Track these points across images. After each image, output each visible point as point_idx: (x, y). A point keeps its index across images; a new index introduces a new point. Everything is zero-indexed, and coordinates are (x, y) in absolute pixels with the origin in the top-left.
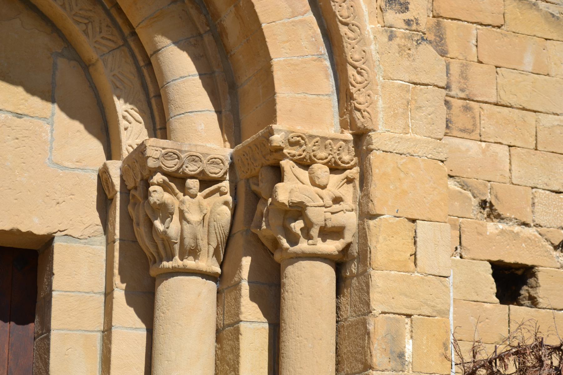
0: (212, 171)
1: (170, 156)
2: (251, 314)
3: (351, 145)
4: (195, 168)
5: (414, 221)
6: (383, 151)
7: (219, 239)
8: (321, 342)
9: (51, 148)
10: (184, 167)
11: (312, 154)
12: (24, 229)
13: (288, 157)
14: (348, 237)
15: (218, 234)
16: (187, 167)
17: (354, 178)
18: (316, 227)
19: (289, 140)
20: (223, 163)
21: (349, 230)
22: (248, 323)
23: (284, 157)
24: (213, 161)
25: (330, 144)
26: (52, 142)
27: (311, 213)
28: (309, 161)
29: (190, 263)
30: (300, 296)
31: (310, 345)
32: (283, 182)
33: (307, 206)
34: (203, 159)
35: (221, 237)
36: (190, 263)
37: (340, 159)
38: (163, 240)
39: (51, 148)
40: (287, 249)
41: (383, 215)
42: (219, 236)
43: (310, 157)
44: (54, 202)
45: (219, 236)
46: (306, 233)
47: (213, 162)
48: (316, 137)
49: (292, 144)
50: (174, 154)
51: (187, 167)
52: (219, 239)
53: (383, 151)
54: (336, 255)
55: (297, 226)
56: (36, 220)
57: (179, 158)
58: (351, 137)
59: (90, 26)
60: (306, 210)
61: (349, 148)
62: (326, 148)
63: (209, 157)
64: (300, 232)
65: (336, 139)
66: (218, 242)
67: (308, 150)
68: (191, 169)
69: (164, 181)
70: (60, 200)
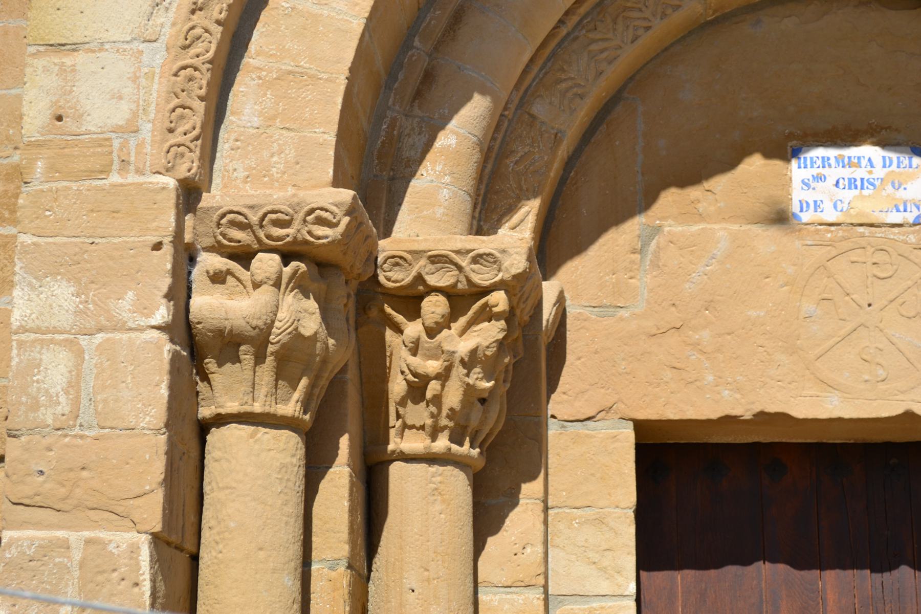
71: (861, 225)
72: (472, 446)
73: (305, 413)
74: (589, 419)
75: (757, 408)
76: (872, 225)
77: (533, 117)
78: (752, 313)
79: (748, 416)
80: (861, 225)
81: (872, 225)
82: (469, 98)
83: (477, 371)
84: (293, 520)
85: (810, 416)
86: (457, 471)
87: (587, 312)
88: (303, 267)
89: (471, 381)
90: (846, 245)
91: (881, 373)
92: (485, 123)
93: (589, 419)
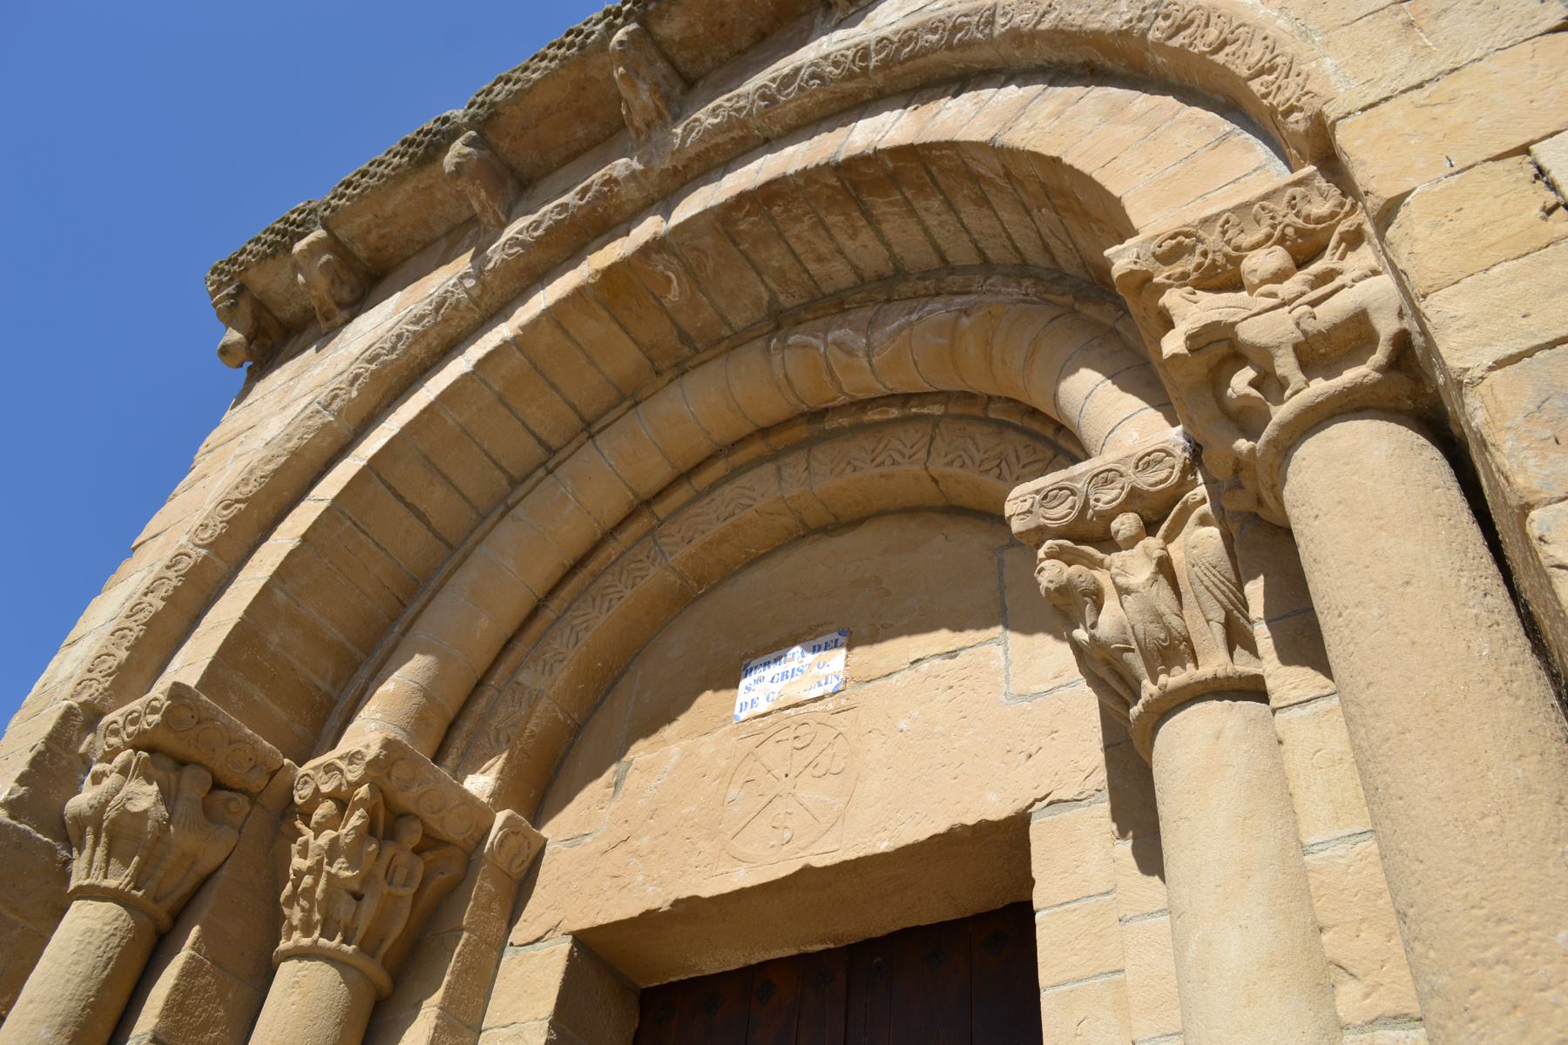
0: (1153, 480)
1: (1055, 497)
2: (830, 424)
3: (1321, 182)
4: (1114, 493)
5: (1524, 150)
6: (1363, 110)
7: (1222, 597)
8: (1409, 589)
9: (1007, 678)
10: (1092, 502)
11: (1228, 249)
12: (970, 820)
13: (1170, 286)
14: (1386, 327)
15: (1212, 588)
16: (1097, 500)
17: (1360, 225)
18: (1280, 352)
19: (1154, 254)
20: (1169, 454)
21: (1378, 309)
22: (1296, 708)
23: (1161, 289)
24: (1146, 462)
25: (1263, 208)
26: (1007, 669)
27: (1250, 332)
28: (1229, 267)
29: (1178, 677)
30: (1316, 523)
31: (1375, 612)
32: (1173, 327)
33: (1234, 324)
34: (1122, 469)
35: (1223, 593)
36: (1178, 677)
37: (1307, 219)
38: (1108, 663)
39: (1007, 678)
40: (1252, 451)
41: (1410, 192)
42: (1217, 592)
43: (1226, 255)
44: (1023, 756)
45: (1217, 592)
46: (1271, 385)
47: (1148, 463)
48: (1218, 215)
49: (1167, 258)
50: (1061, 489)
51: (1097, 500)
52: (1222, 597)
53: (1363, 110)
54: (1376, 384)
55: (1241, 382)
56: (992, 797)
57: (1073, 493)
58: (1310, 169)
59: (1004, 464)
60: (1236, 334)
61: (1319, 189)
62: (1258, 222)
63: (1134, 460)
64: (1254, 392)
65: (1274, 192)
66: (1224, 608)
67: (1210, 248)
68: (1108, 498)
69: (1060, 546)
70: (1033, 750)
71: (788, 708)
72: (345, 941)
73: (137, 888)
74: (538, 940)
75: (672, 898)
76: (797, 705)
77: (519, 684)
78: (686, 811)
79: (666, 908)
80: (788, 708)
81: (797, 705)
82: (411, 658)
83: (341, 862)
84: (77, 980)
85: (716, 893)
86: (326, 967)
87: (559, 846)
88: (145, 754)
89: (333, 871)
90: (777, 728)
91: (787, 835)
92: (430, 673)
93: (538, 940)
